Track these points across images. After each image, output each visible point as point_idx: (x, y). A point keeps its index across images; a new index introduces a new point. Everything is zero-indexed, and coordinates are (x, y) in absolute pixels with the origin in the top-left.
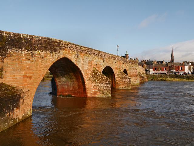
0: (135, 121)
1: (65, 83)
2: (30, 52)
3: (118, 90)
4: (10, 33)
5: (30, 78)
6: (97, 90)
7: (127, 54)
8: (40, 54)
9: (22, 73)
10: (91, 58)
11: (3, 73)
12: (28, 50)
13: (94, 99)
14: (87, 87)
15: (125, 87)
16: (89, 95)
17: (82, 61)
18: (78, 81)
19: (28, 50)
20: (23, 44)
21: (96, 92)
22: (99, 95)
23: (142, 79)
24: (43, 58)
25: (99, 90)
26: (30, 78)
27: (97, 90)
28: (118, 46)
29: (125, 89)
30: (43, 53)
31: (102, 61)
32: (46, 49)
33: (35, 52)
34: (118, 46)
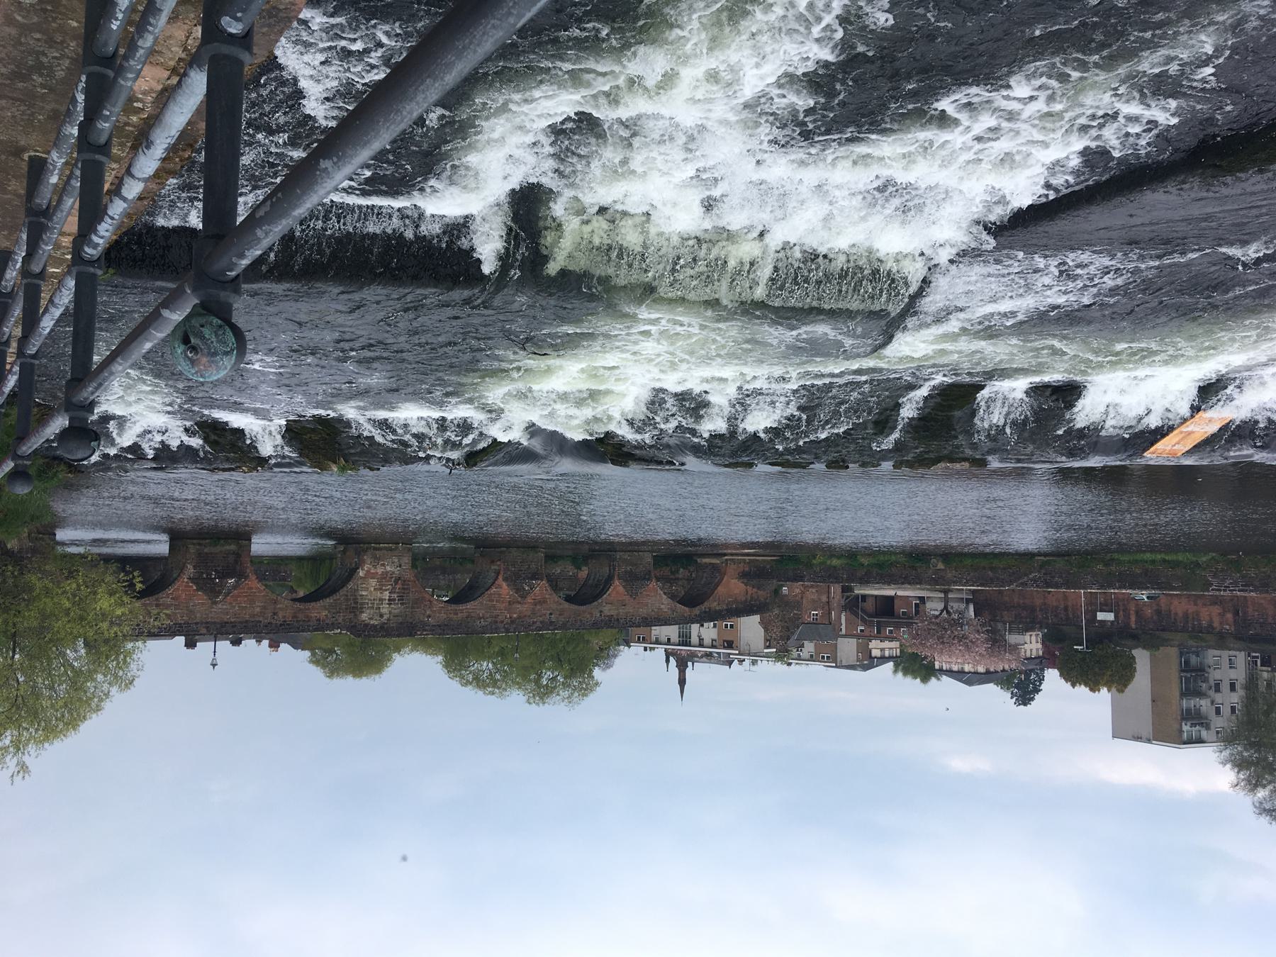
28: (214, 665)
34: (214, 665)
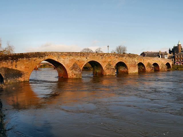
0: (96, 94)
1: (122, 69)
2: (28, 59)
3: (106, 75)
4: (19, 54)
5: (28, 68)
6: (73, 74)
7: (180, 44)
8: (33, 59)
9: (24, 66)
10: (72, 58)
11: (17, 66)
12: (27, 58)
13: (72, 79)
14: (68, 73)
15: (111, 74)
16: (69, 77)
17: (63, 60)
18: (64, 70)
19: (27, 58)
20: (24, 56)
21: (73, 76)
22: (75, 77)
23: (152, 69)
24: (35, 60)
25: (75, 75)
26: (28, 68)
27: (73, 74)
28: (108, 46)
29: (111, 76)
30: (35, 58)
31: (85, 58)
32: (36, 57)
33: (30, 59)
34: (108, 46)
